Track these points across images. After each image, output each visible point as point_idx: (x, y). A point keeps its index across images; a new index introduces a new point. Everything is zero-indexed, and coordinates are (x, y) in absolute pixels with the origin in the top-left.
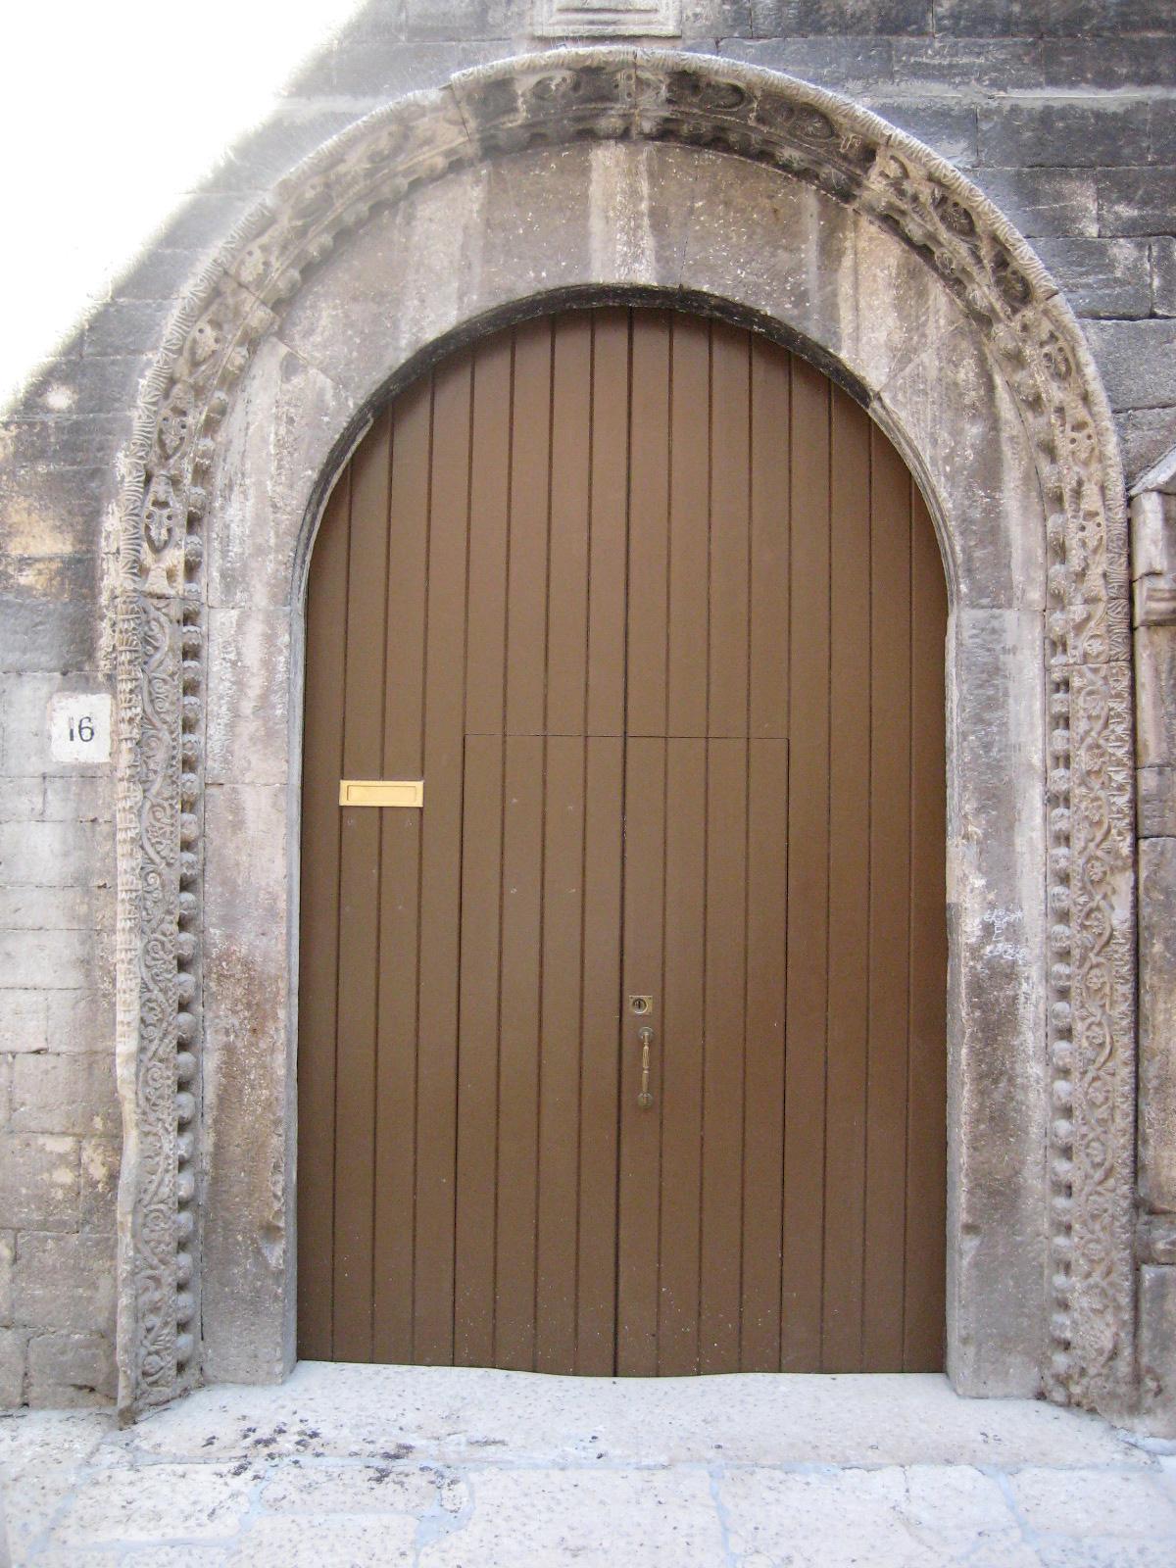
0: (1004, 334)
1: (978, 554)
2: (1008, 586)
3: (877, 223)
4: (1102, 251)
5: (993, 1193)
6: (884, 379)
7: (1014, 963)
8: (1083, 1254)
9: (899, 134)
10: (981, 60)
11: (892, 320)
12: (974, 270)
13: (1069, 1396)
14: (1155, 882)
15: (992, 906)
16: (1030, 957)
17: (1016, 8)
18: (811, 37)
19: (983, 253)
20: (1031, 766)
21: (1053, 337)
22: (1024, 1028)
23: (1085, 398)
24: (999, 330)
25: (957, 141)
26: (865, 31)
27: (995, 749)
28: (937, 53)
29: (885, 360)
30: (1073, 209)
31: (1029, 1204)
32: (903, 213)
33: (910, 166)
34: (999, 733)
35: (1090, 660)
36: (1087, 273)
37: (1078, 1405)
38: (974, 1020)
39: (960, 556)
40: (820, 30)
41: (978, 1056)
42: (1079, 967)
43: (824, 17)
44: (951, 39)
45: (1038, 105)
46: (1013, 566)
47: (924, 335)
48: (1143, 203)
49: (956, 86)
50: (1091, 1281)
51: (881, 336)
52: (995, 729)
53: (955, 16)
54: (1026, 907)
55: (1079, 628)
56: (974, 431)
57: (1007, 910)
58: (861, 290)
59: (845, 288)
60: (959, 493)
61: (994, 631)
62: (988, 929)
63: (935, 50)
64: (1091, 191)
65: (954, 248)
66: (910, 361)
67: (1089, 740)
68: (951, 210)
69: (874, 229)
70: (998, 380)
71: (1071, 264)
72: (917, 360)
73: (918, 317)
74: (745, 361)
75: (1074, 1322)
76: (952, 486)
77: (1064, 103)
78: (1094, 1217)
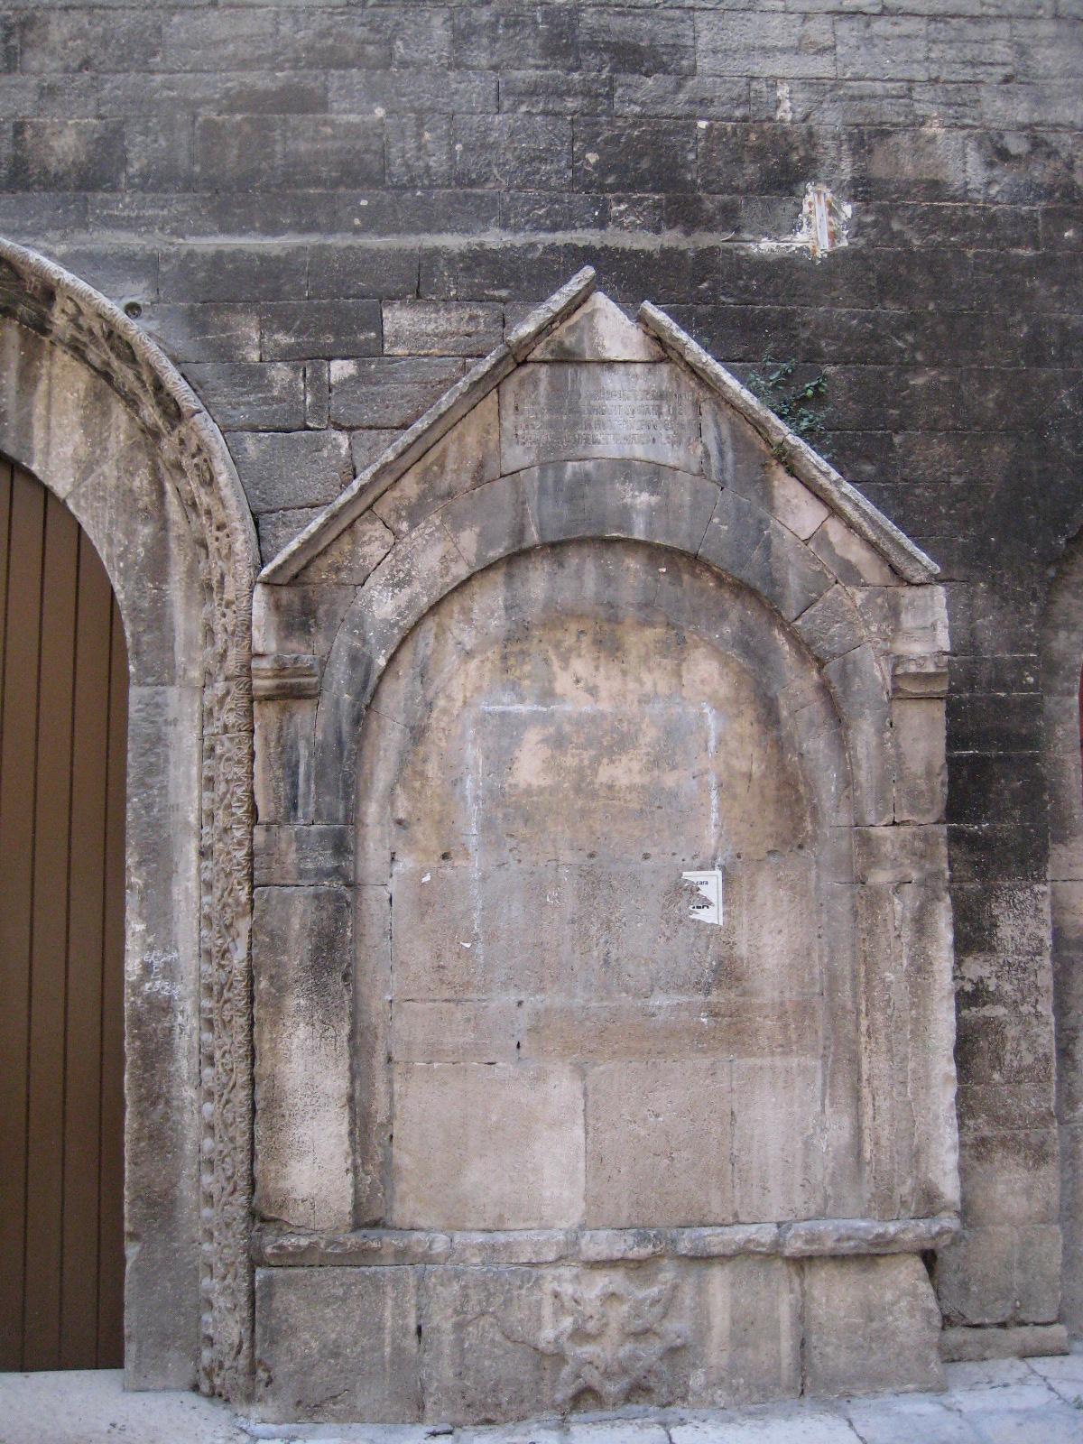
0: (168, 445)
1: (146, 638)
2: (172, 666)
3: (70, 352)
4: (262, 373)
5: (151, 1204)
6: (69, 488)
7: (171, 997)
8: (221, 1259)
9: (68, 277)
10: (165, 212)
11: (78, 436)
12: (139, 392)
13: (213, 1388)
14: (262, 927)
15: (151, 948)
16: (185, 995)
17: (197, 169)
18: (19, 194)
19: (145, 378)
20: (187, 823)
21: (199, 450)
22: (179, 1056)
23: (221, 500)
24: (165, 444)
25: (140, 282)
26: (66, 188)
27: (156, 810)
28: (126, 206)
29: (71, 471)
30: (238, 337)
31: (184, 1213)
32: (85, 345)
33: (82, 305)
34: (160, 795)
35: (230, 730)
36: (247, 393)
37: (220, 1395)
38: (134, 1049)
39: (129, 640)
40: (27, 188)
41: (139, 1082)
42: (218, 1001)
43: (30, 176)
44: (140, 194)
45: (211, 250)
46: (176, 649)
47: (106, 449)
48: (299, 332)
49: (141, 235)
50: (226, 1282)
51: (69, 450)
52: (156, 792)
53: (144, 176)
54: (181, 949)
55: (221, 701)
56: (145, 531)
57: (165, 951)
58: (53, 410)
59: (39, 410)
60: (131, 585)
61: (157, 705)
62: (147, 968)
63: (125, 203)
64: (254, 322)
65: (124, 373)
66: (93, 471)
67: (226, 801)
68: (117, 342)
69: (67, 358)
70: (169, 487)
71: (235, 385)
72: (99, 471)
73: (101, 433)
74: (9, 474)
75: (215, 1320)
76: (125, 580)
77: (234, 248)
78: (228, 1225)
